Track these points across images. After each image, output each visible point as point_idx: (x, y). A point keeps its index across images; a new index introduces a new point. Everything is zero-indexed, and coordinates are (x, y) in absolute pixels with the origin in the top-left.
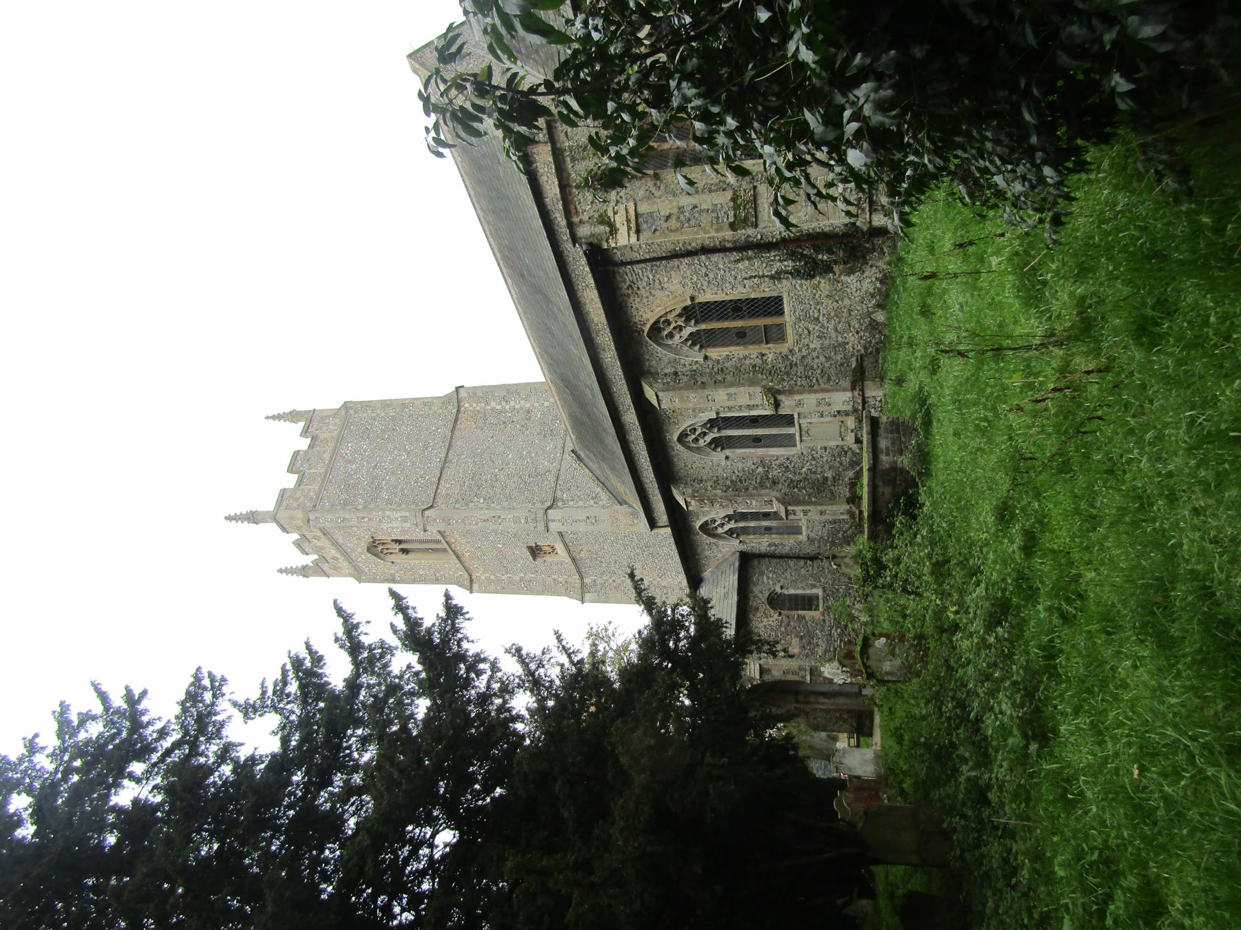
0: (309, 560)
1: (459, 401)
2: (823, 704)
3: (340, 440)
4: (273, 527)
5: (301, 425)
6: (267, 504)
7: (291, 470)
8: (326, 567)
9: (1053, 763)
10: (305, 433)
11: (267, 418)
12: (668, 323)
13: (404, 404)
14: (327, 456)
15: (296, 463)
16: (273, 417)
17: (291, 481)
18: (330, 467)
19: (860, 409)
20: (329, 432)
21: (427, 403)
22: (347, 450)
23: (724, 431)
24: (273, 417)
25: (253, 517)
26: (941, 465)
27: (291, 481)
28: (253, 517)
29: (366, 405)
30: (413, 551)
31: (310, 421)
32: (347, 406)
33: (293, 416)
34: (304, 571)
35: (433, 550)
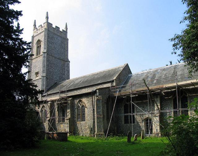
0: (37, 26)
1: (67, 61)
2: (150, 127)
3: (61, 37)
5: (64, 30)
7: (56, 27)
8: (36, 30)
9: (131, 128)
10: (63, 30)
12: (82, 103)
13: (67, 50)
14: (58, 34)
15: (57, 28)
17: (54, 26)
18: (55, 34)
20: (63, 35)
22: (59, 38)
25: (47, 18)
26: (168, 116)
27: (54, 26)
28: (47, 18)
30: (38, 49)
31: (65, 32)
34: (35, 25)
35: (38, 53)
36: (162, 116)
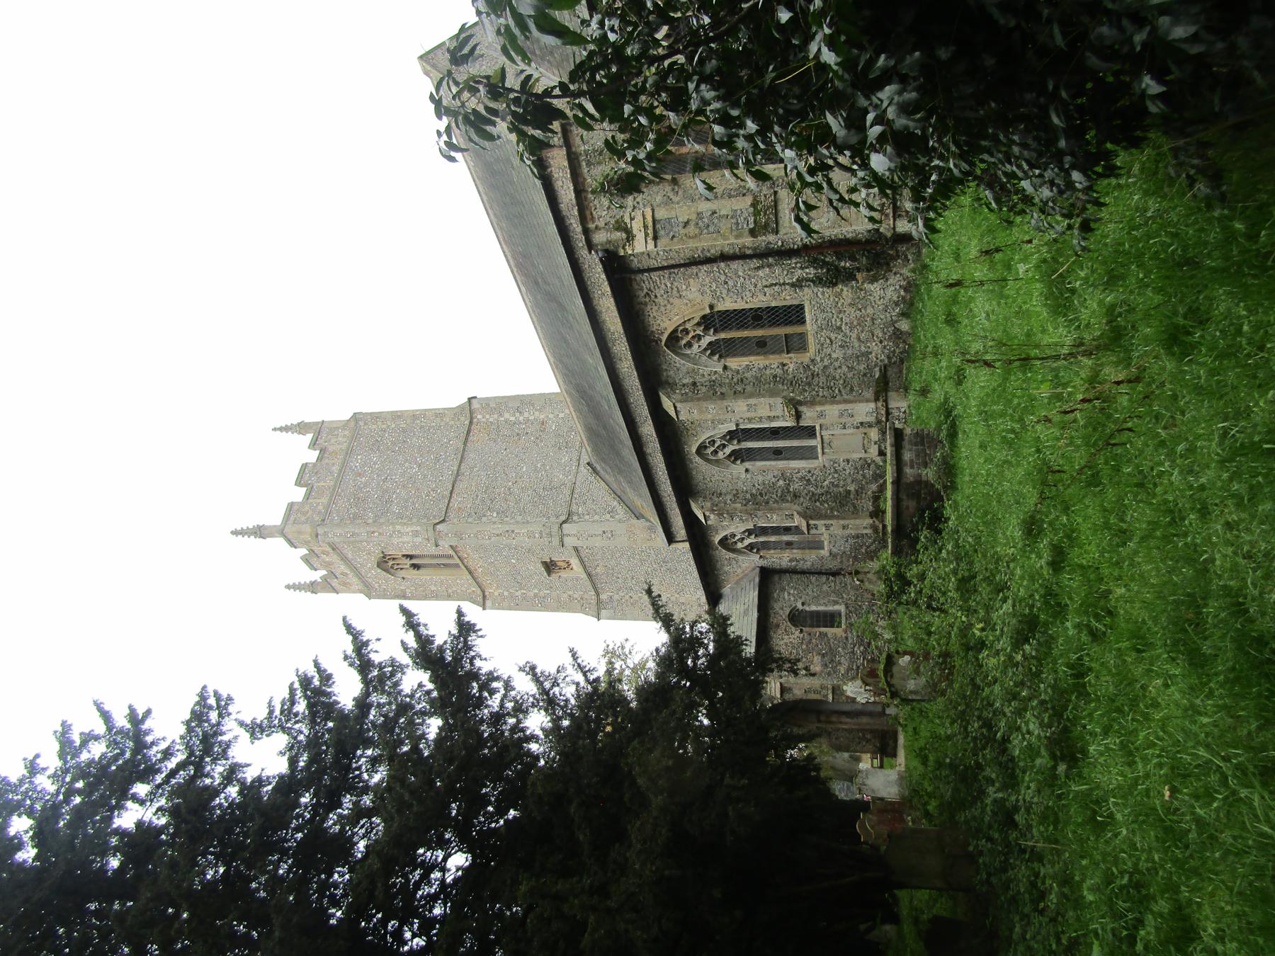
0: (317, 575)
1: (471, 412)
3: (349, 453)
4: (280, 541)
5: (310, 436)
6: (275, 518)
7: (299, 483)
8: (335, 583)
9: (1082, 785)
10: (313, 445)
11: (275, 429)
12: (686, 332)
13: (415, 416)
14: (336, 469)
15: (304, 476)
16: (281, 429)
17: (299, 494)
18: (339, 480)
19: (883, 421)
20: (338, 444)
21: (439, 414)
22: (357, 462)
23: (743, 443)
24: (281, 429)
25: (260, 532)
26: (967, 479)
27: (299, 494)
28: (260, 532)
29: (376, 417)
30: (424, 566)
31: (318, 432)
32: (356, 417)
33: (301, 428)
34: (312, 587)
35: (445, 565)
36: (716, 391)
